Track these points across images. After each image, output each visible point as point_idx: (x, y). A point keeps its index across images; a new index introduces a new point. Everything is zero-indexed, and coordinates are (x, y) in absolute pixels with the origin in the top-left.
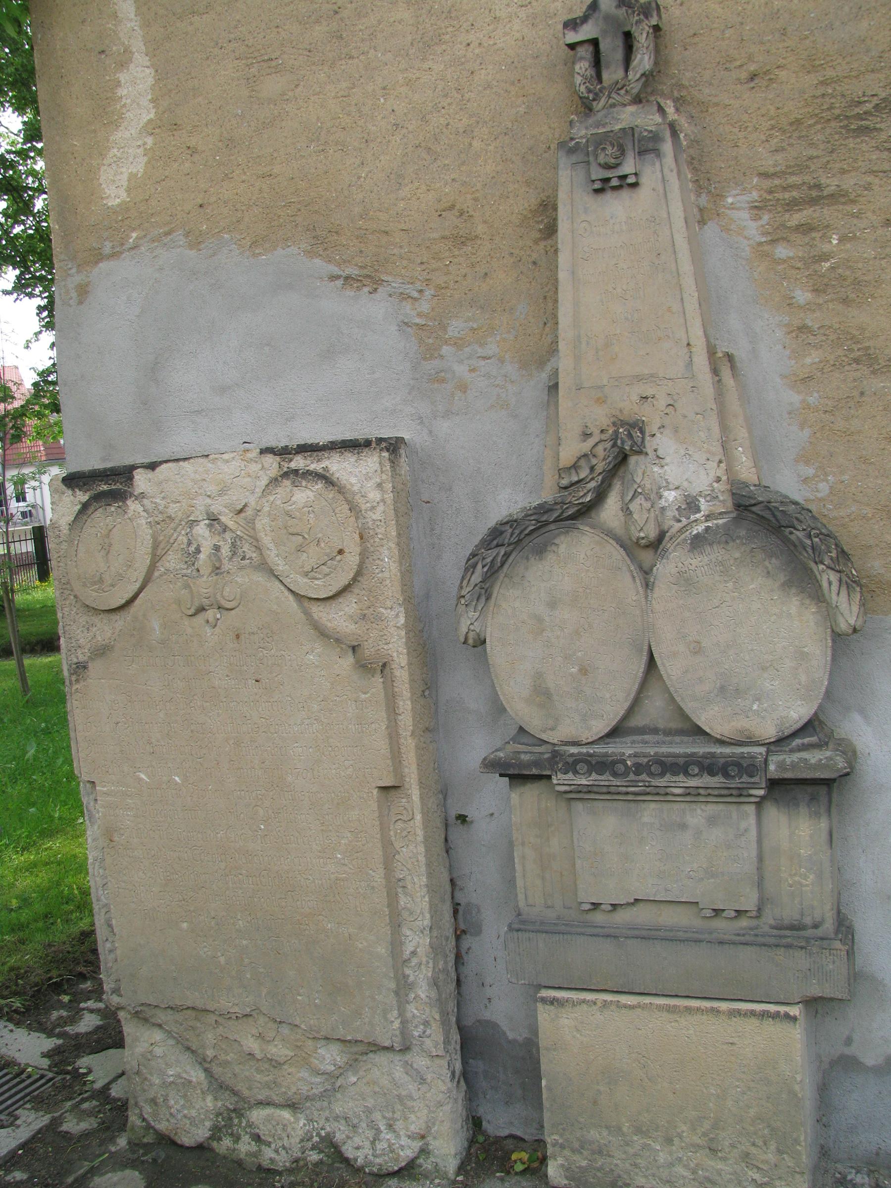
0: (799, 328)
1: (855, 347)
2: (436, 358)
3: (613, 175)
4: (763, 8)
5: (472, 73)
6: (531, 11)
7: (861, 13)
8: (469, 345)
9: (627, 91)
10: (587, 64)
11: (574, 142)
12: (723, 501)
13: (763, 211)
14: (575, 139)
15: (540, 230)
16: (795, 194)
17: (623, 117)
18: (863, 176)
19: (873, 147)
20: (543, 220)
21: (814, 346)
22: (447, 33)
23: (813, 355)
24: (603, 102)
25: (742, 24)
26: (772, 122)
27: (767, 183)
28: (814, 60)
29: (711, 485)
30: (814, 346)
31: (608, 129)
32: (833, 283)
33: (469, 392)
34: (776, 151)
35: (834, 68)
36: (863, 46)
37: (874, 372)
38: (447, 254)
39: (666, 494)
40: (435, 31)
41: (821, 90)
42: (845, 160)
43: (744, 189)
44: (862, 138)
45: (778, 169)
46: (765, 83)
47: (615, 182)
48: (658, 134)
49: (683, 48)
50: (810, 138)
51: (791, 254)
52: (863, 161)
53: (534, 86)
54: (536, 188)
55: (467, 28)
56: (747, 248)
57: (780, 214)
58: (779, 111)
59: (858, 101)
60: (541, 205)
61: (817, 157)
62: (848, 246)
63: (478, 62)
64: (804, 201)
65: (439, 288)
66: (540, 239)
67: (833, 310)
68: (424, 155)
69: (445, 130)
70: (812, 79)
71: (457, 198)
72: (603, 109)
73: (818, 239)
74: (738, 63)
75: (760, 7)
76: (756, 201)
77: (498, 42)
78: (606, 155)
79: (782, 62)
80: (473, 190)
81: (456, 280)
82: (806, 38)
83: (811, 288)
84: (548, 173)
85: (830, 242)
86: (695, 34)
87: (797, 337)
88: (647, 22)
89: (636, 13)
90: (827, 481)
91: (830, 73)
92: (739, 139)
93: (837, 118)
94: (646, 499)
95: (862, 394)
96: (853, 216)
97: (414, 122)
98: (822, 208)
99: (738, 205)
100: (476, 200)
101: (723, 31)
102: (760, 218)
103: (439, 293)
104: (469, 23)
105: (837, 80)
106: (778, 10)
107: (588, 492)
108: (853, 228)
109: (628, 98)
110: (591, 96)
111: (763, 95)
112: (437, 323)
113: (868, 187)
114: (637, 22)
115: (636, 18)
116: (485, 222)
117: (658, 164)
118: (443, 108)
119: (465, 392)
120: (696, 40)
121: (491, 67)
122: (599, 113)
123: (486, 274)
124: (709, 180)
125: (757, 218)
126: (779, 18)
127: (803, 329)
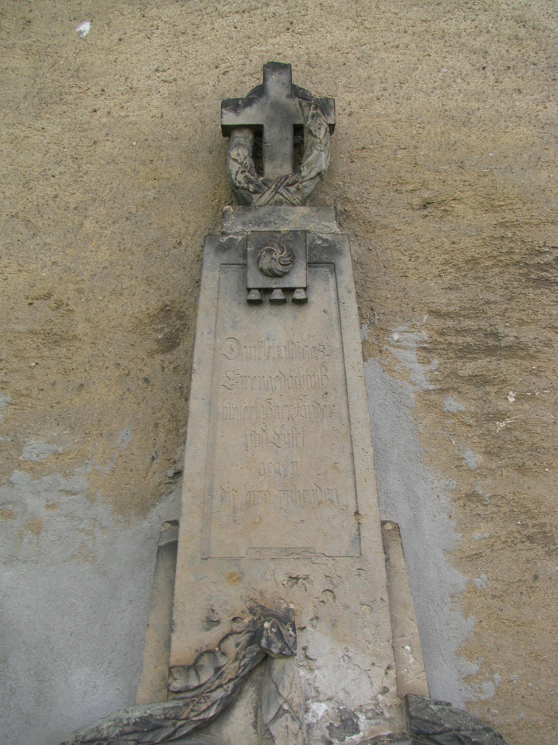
0: (467, 496)
1: (530, 523)
2: (4, 484)
3: (277, 286)
4: (438, 137)
5: (95, 142)
6: (175, 88)
7: (540, 163)
8: (50, 473)
9: (298, 189)
10: (246, 153)
11: (225, 238)
12: (390, 720)
13: (434, 355)
14: (228, 235)
15: (158, 341)
16: (469, 339)
17: (291, 218)
18: (543, 330)
19: (554, 301)
20: (163, 328)
21: (484, 518)
22: (71, 94)
23: (483, 529)
24: (267, 196)
25: (416, 148)
26: (446, 256)
27: (438, 324)
28: (494, 199)
29: (375, 698)
30: (484, 518)
31: (272, 229)
32: (509, 446)
33: (43, 534)
34: (450, 289)
35: (514, 212)
36: (543, 196)
37: (548, 553)
38: (34, 353)
39: (314, 706)
40: (56, 88)
41: (500, 232)
42: (524, 310)
43: (413, 326)
44: (542, 290)
45: (452, 309)
46: (439, 214)
47: (278, 295)
48: (335, 245)
49: (349, 160)
50: (487, 280)
51: (462, 408)
52: (544, 314)
53: (170, 170)
54: (159, 289)
55: (95, 93)
56: (412, 396)
57: (452, 360)
58: (454, 246)
59: (538, 251)
60: (162, 310)
61: (495, 303)
62: (526, 406)
63: (104, 132)
64: (480, 349)
65: (17, 394)
66: (157, 352)
67: (507, 477)
68: (21, 227)
69: (51, 202)
70: (490, 219)
71: (56, 285)
72: (266, 204)
73: (493, 394)
74: (410, 187)
75: (436, 135)
76: (425, 342)
77: (132, 114)
78: (273, 258)
79: (458, 194)
80: (78, 279)
81: (41, 387)
82: (485, 175)
83: (483, 450)
84: (175, 272)
85: (507, 399)
86: (364, 148)
87: (465, 505)
88: (324, 118)
89: (313, 106)
90: (493, 680)
91: (510, 216)
92: (408, 269)
93: (517, 263)
94: (293, 719)
95: (536, 577)
96: (531, 372)
97: (13, 187)
98: (499, 360)
99: (404, 344)
100: (80, 291)
101: (395, 151)
102: (429, 362)
103: (18, 401)
104: (99, 88)
105: (516, 225)
106: (456, 142)
107: (213, 704)
108: (532, 387)
109: (298, 198)
110: (252, 188)
111: (437, 226)
112: (9, 440)
113: (548, 343)
114: (313, 116)
115: (312, 112)
116: (88, 320)
117: (332, 282)
118: (53, 176)
119: (38, 533)
120: (364, 154)
121: (119, 140)
122: (262, 208)
123: (82, 386)
124: (372, 309)
125: (425, 361)
126: (455, 150)
127: (472, 496)
